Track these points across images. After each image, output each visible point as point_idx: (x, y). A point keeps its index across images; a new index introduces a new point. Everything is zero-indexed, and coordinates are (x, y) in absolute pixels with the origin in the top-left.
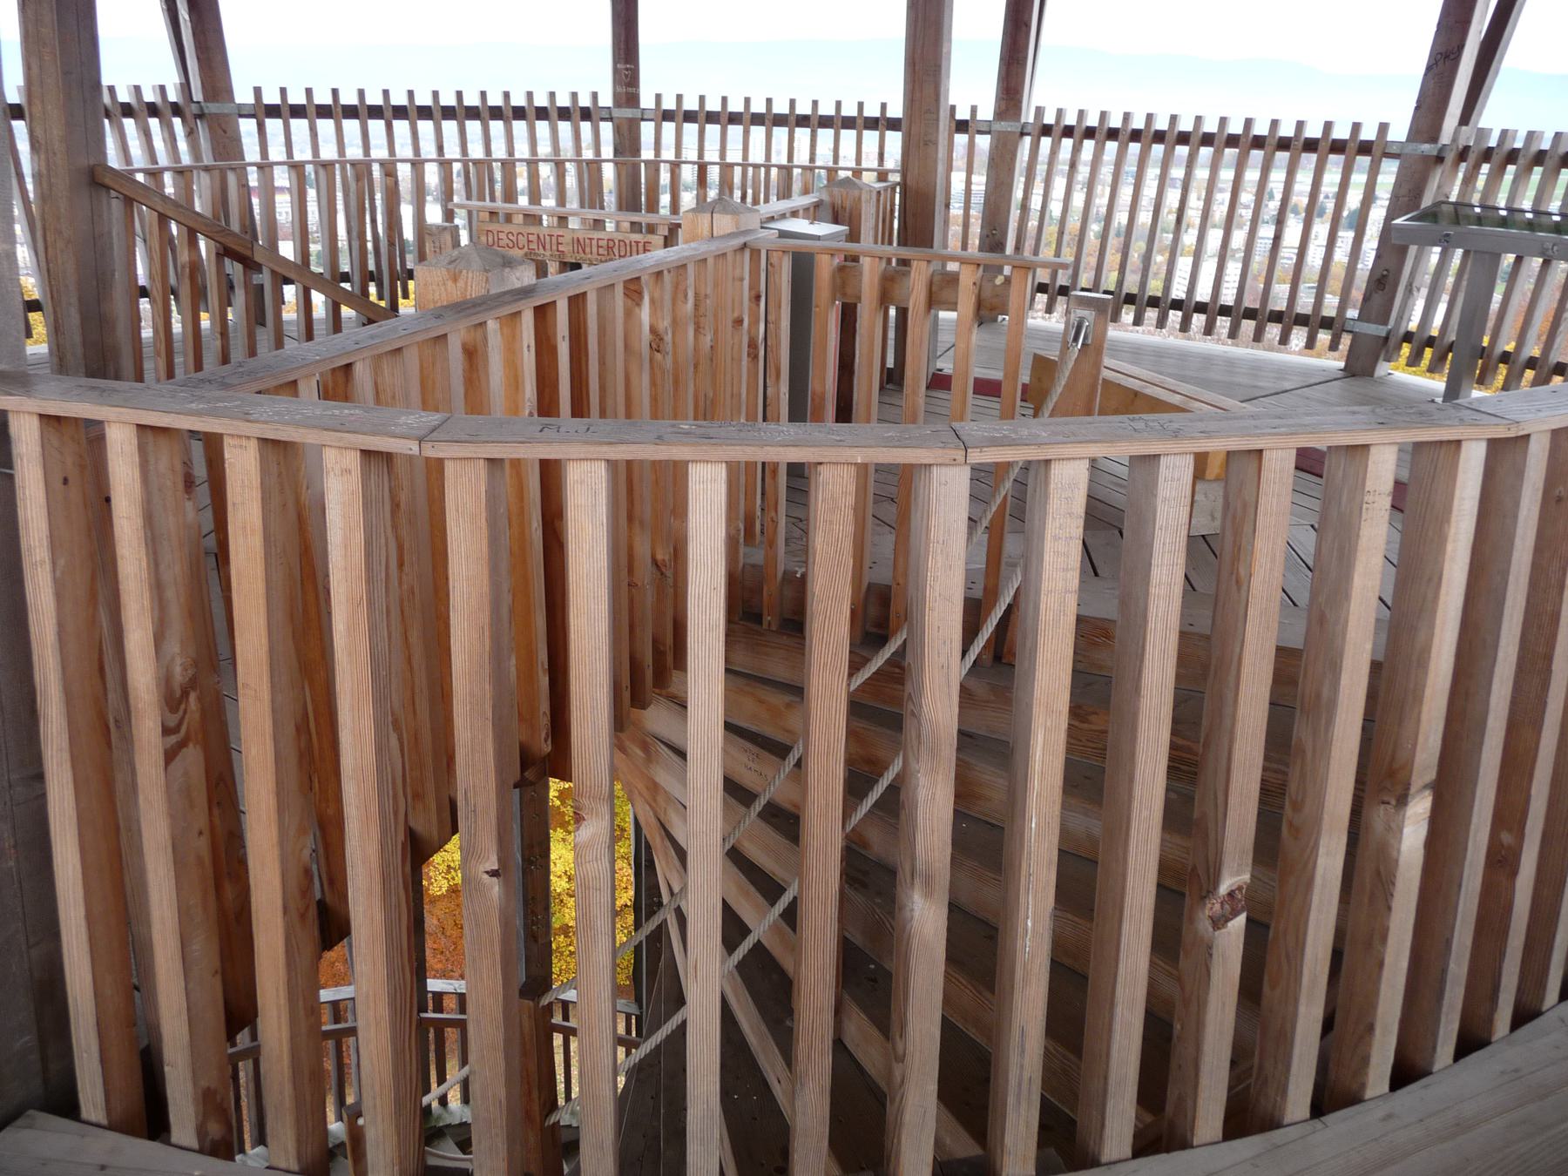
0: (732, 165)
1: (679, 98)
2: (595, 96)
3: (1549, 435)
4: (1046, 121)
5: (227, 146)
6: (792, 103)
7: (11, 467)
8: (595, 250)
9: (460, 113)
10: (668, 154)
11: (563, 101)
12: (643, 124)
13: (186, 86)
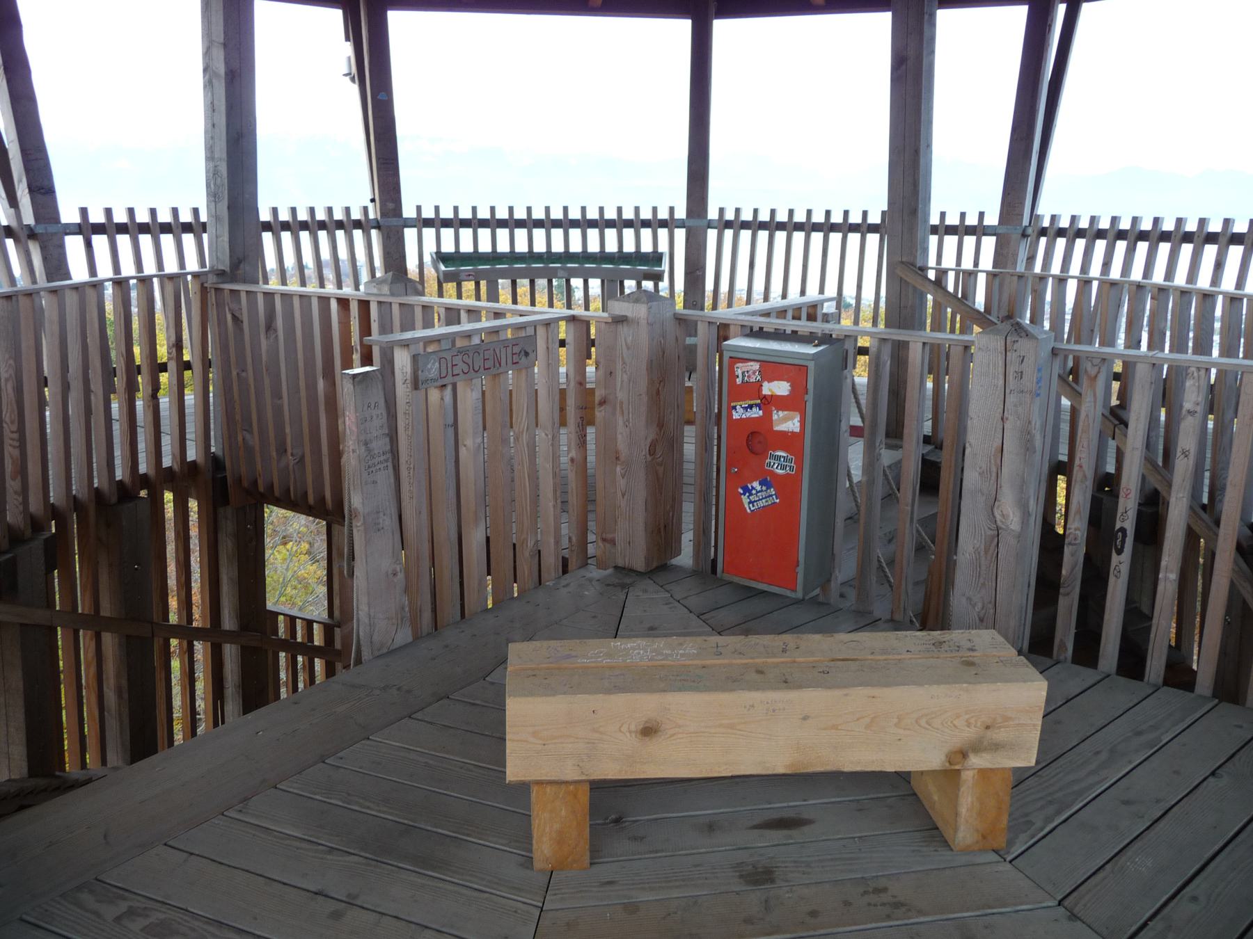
0: (150, 278)
1: (637, 209)
2: (672, 210)
3: (584, 796)
4: (1061, 225)
5: (57, 266)
6: (456, 209)
7: (529, 810)
10: (1056, 269)
12: (407, 231)
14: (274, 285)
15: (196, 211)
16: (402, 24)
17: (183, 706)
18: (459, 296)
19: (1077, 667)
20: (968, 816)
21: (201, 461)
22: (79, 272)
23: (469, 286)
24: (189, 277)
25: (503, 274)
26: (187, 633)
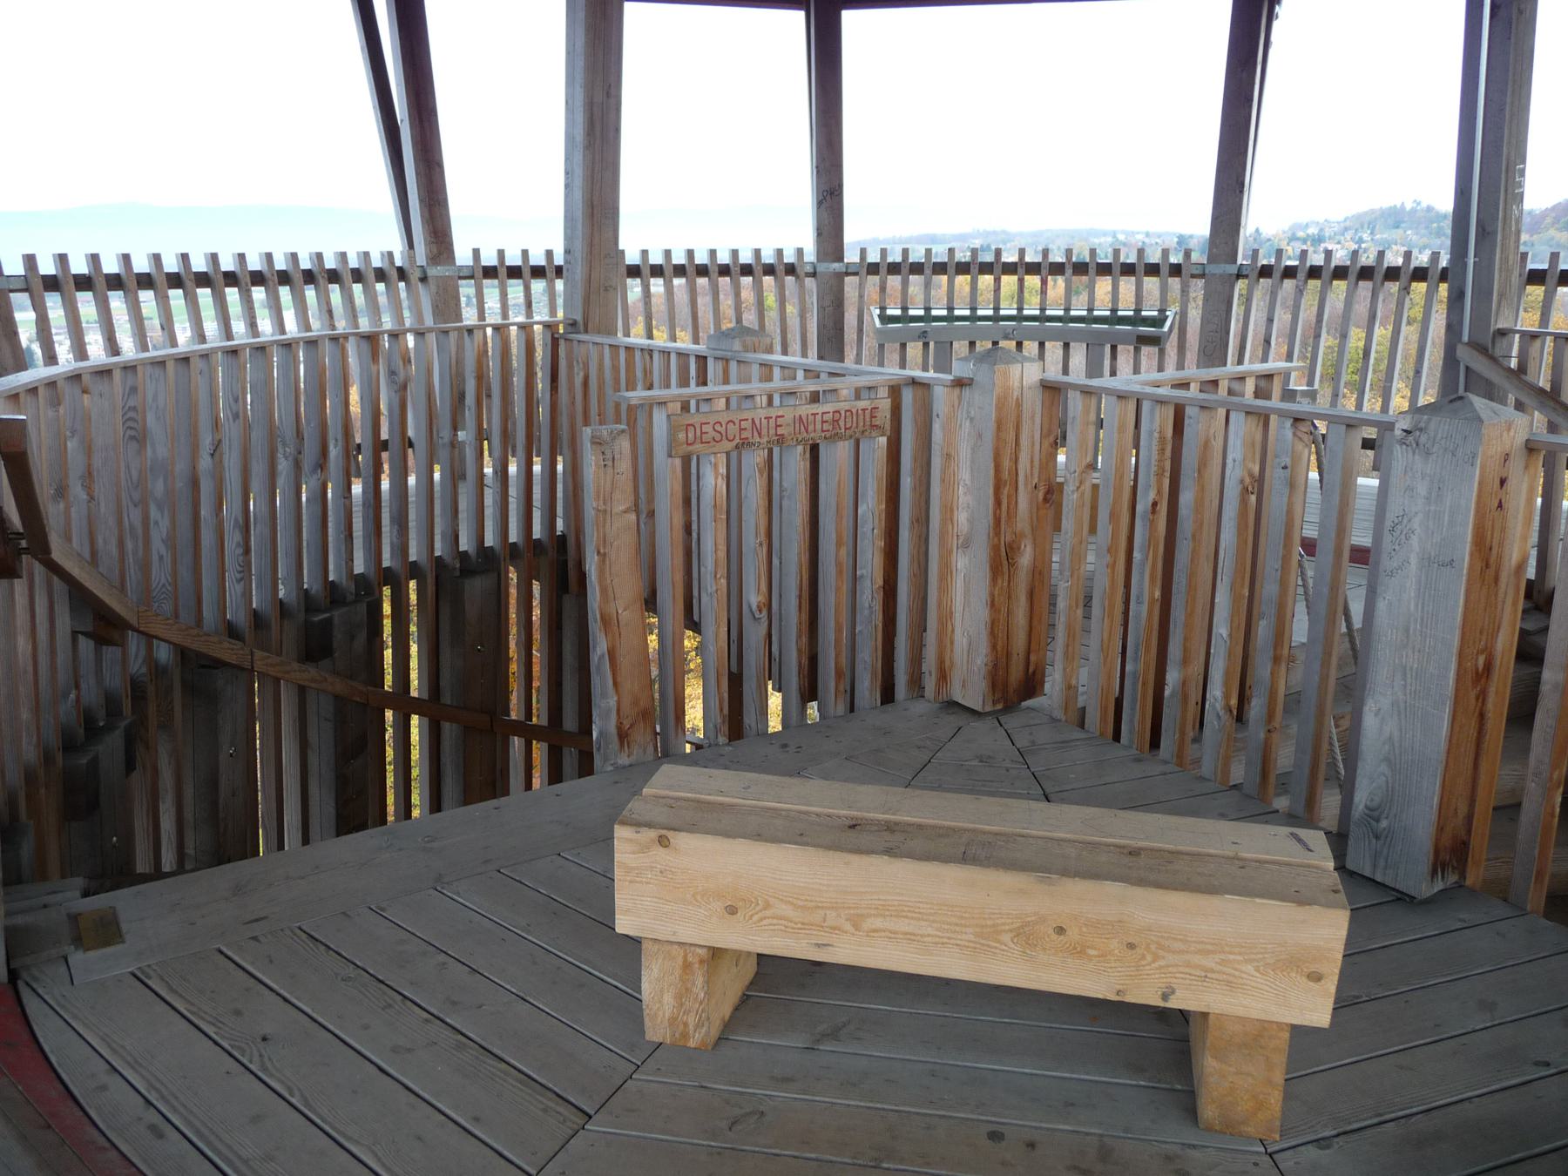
5: (447, 305)
8: (819, 426)
9: (216, 279)
11: (679, 258)
13: (411, 258)
14: (637, 338)
15: (549, 254)
16: (851, 19)
17: (396, 803)
18: (903, 365)
19: (124, 927)
20: (1239, 1086)
21: (545, 540)
22: (469, 316)
23: (915, 350)
24: (489, 331)
25: (1124, 339)
26: (529, 732)
